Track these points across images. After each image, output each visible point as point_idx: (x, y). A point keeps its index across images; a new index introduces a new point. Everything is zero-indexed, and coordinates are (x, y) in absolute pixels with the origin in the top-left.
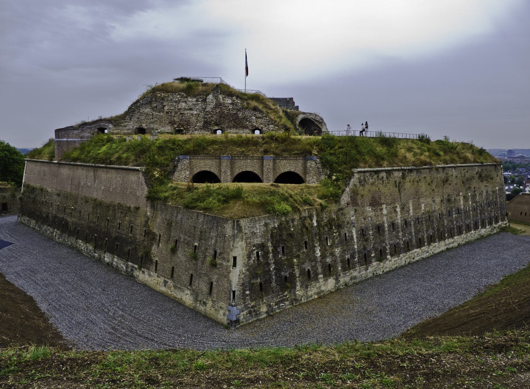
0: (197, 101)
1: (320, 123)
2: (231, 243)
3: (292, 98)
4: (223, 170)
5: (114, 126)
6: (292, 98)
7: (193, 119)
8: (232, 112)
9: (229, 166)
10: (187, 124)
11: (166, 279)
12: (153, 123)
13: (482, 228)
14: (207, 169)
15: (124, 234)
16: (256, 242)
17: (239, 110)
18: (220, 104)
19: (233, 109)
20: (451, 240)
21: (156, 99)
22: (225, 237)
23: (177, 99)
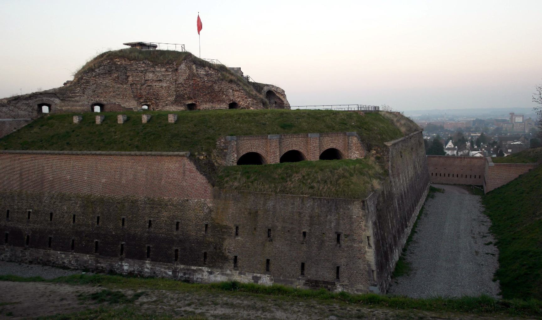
1: (282, 95)
3: (240, 68)
5: (62, 100)
6: (240, 68)
7: (163, 92)
9: (278, 145)
10: (155, 98)
15: (163, 233)
17: (215, 83)
18: (194, 75)
21: (116, 68)
23: (142, 69)
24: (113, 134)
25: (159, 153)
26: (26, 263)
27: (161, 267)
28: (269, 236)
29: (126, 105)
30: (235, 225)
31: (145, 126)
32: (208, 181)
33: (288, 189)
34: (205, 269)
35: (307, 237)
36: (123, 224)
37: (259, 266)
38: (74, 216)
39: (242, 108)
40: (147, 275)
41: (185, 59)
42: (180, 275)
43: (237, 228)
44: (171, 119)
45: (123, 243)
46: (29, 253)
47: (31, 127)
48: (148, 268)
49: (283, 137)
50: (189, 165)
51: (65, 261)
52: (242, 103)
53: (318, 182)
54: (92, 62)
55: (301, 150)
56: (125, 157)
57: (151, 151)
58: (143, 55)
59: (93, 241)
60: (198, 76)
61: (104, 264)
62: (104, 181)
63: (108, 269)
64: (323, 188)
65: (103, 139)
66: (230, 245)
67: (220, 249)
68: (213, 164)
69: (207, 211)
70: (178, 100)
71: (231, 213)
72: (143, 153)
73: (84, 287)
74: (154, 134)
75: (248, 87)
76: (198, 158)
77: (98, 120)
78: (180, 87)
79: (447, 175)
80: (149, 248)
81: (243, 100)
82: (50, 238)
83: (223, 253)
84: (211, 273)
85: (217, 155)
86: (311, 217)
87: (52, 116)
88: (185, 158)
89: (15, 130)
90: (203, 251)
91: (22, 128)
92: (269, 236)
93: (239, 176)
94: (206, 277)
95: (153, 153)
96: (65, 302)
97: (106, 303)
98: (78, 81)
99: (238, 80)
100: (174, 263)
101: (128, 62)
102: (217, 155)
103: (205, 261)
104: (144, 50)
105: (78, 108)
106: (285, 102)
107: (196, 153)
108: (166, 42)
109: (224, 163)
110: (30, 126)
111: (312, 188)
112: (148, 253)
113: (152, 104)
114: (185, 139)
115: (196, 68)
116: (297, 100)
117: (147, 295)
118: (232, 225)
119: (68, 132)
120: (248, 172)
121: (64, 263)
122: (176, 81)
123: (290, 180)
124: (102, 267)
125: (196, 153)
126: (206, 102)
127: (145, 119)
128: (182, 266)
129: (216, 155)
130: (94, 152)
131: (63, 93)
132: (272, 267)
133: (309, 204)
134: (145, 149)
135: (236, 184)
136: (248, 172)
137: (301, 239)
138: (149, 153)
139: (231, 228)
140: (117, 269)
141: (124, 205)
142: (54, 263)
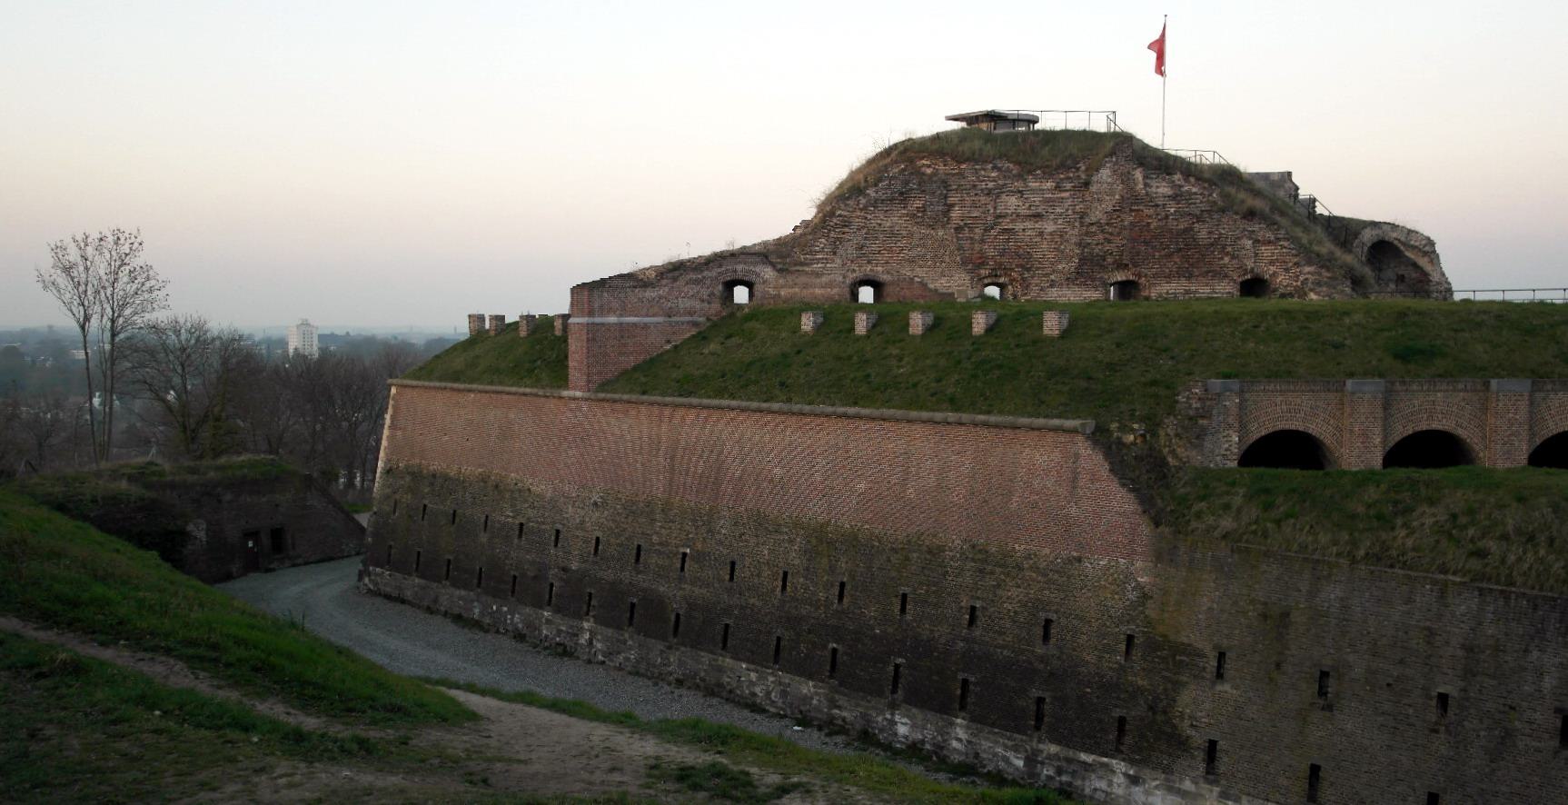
0: (1058, 188)
1: (1425, 254)
3: (1289, 174)
6: (1289, 174)
8: (1172, 224)
9: (1380, 413)
12: (912, 261)
15: (1003, 647)
17: (1199, 219)
19: (1180, 214)
23: (991, 185)
24: (894, 362)
25: (1010, 419)
26: (669, 684)
27: (996, 742)
28: (1322, 692)
29: (941, 284)
30: (1215, 647)
31: (978, 342)
32: (1140, 509)
33: (1394, 553)
34: (1119, 766)
35: (1450, 713)
36: (903, 610)
37: (1283, 781)
38: (785, 574)
39: (1283, 296)
40: (956, 758)
41: (1112, 154)
42: (1047, 771)
43: (1221, 656)
44: (1052, 324)
45: (899, 661)
46: (677, 660)
47: (704, 338)
48: (959, 740)
49: (1398, 386)
50: (1091, 459)
51: (757, 690)
52: (1282, 280)
53: (1505, 537)
54: (859, 170)
55: (1460, 432)
56: (918, 427)
57: (989, 413)
58: (999, 145)
59: (825, 647)
60: (1150, 200)
61: (848, 713)
62: (862, 486)
63: (858, 727)
64: (1520, 559)
65: (868, 376)
66: (1199, 707)
67: (1165, 712)
68: (1164, 463)
69: (1132, 596)
70: (1088, 268)
71: (1206, 610)
72: (965, 417)
73: (685, 749)
74: (1000, 367)
75: (1306, 230)
76: (1120, 442)
77: (861, 324)
78: (1094, 234)
80: (965, 682)
81: (1287, 270)
82: (727, 626)
83: (1174, 727)
84: (1134, 780)
85: (1177, 435)
86: (1469, 649)
87: (753, 313)
88: (1080, 438)
89: (668, 347)
90: (1117, 713)
91: (685, 342)
92: (1322, 692)
93: (1238, 501)
94: (1120, 791)
95: (993, 419)
96: (617, 777)
97: (702, 795)
98: (824, 220)
99: (1274, 208)
100: (1031, 736)
101: (952, 168)
102: (1177, 435)
103: (1119, 740)
104: (1000, 131)
105: (817, 291)
106: (1435, 277)
107: (1114, 426)
108: (1062, 107)
109: (1197, 458)
110: (702, 337)
111: (1481, 554)
112: (963, 696)
113: (1013, 280)
114: (1084, 384)
115: (1145, 177)
116: (1471, 274)
117: (808, 791)
118: (1207, 648)
119: (785, 355)
120: (1267, 491)
121: (754, 694)
122: (1083, 215)
123: (1405, 525)
124: (844, 719)
125: (1114, 426)
126: (1169, 278)
127: (980, 323)
128: (1054, 749)
129: (1172, 433)
130: (841, 410)
131: (779, 254)
133: (1463, 605)
134: (973, 407)
135: (1227, 523)
136: (1267, 491)
137: (1432, 716)
138: (982, 417)
139: (1201, 655)
140: (881, 730)
141: (907, 559)
142: (731, 691)
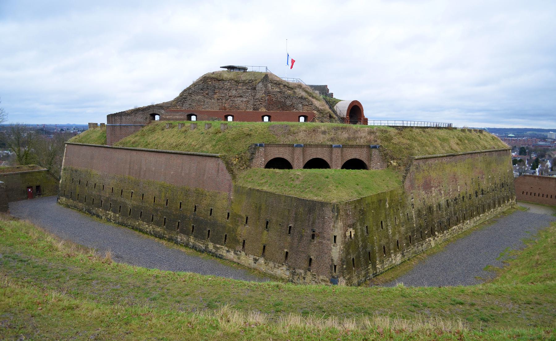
2: (332, 224)
4: (296, 157)
8: (279, 100)
9: (302, 153)
11: (255, 257)
13: (498, 206)
14: (281, 156)
16: (349, 223)
20: (478, 218)
22: (324, 218)
37: (258, 250)
59: (205, 229)
79: (541, 195)
84: (228, 251)
132: (266, 253)
